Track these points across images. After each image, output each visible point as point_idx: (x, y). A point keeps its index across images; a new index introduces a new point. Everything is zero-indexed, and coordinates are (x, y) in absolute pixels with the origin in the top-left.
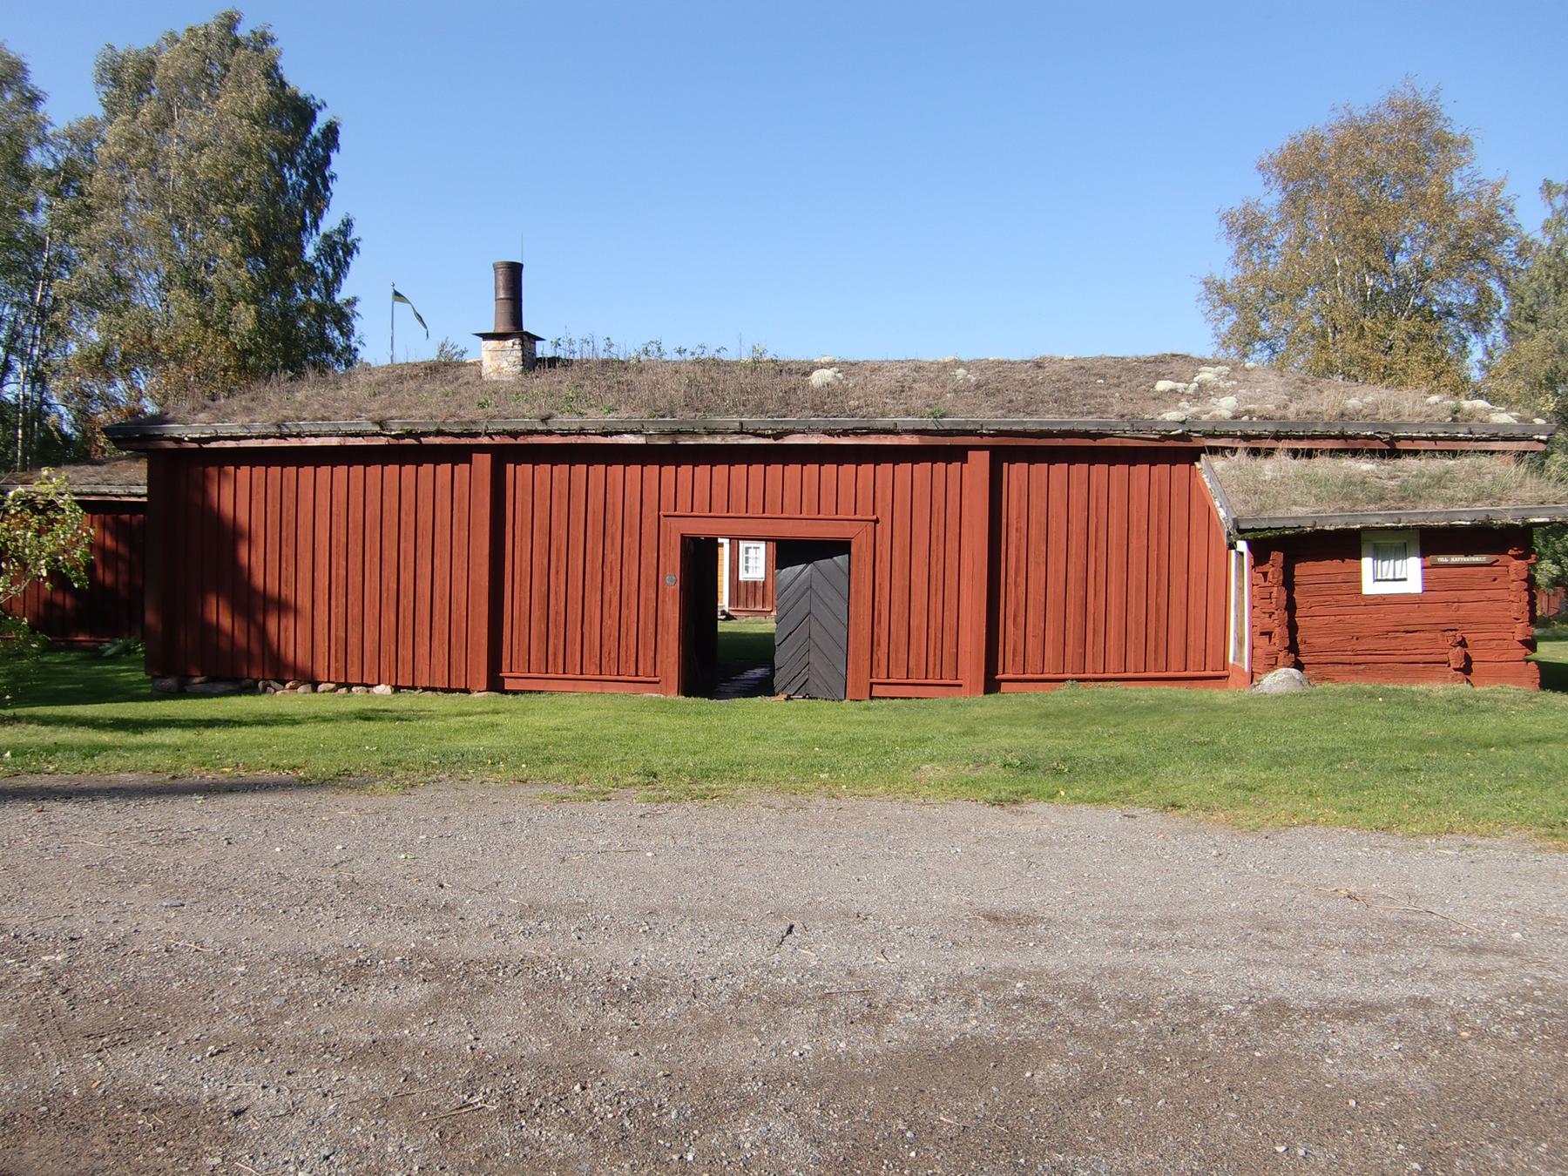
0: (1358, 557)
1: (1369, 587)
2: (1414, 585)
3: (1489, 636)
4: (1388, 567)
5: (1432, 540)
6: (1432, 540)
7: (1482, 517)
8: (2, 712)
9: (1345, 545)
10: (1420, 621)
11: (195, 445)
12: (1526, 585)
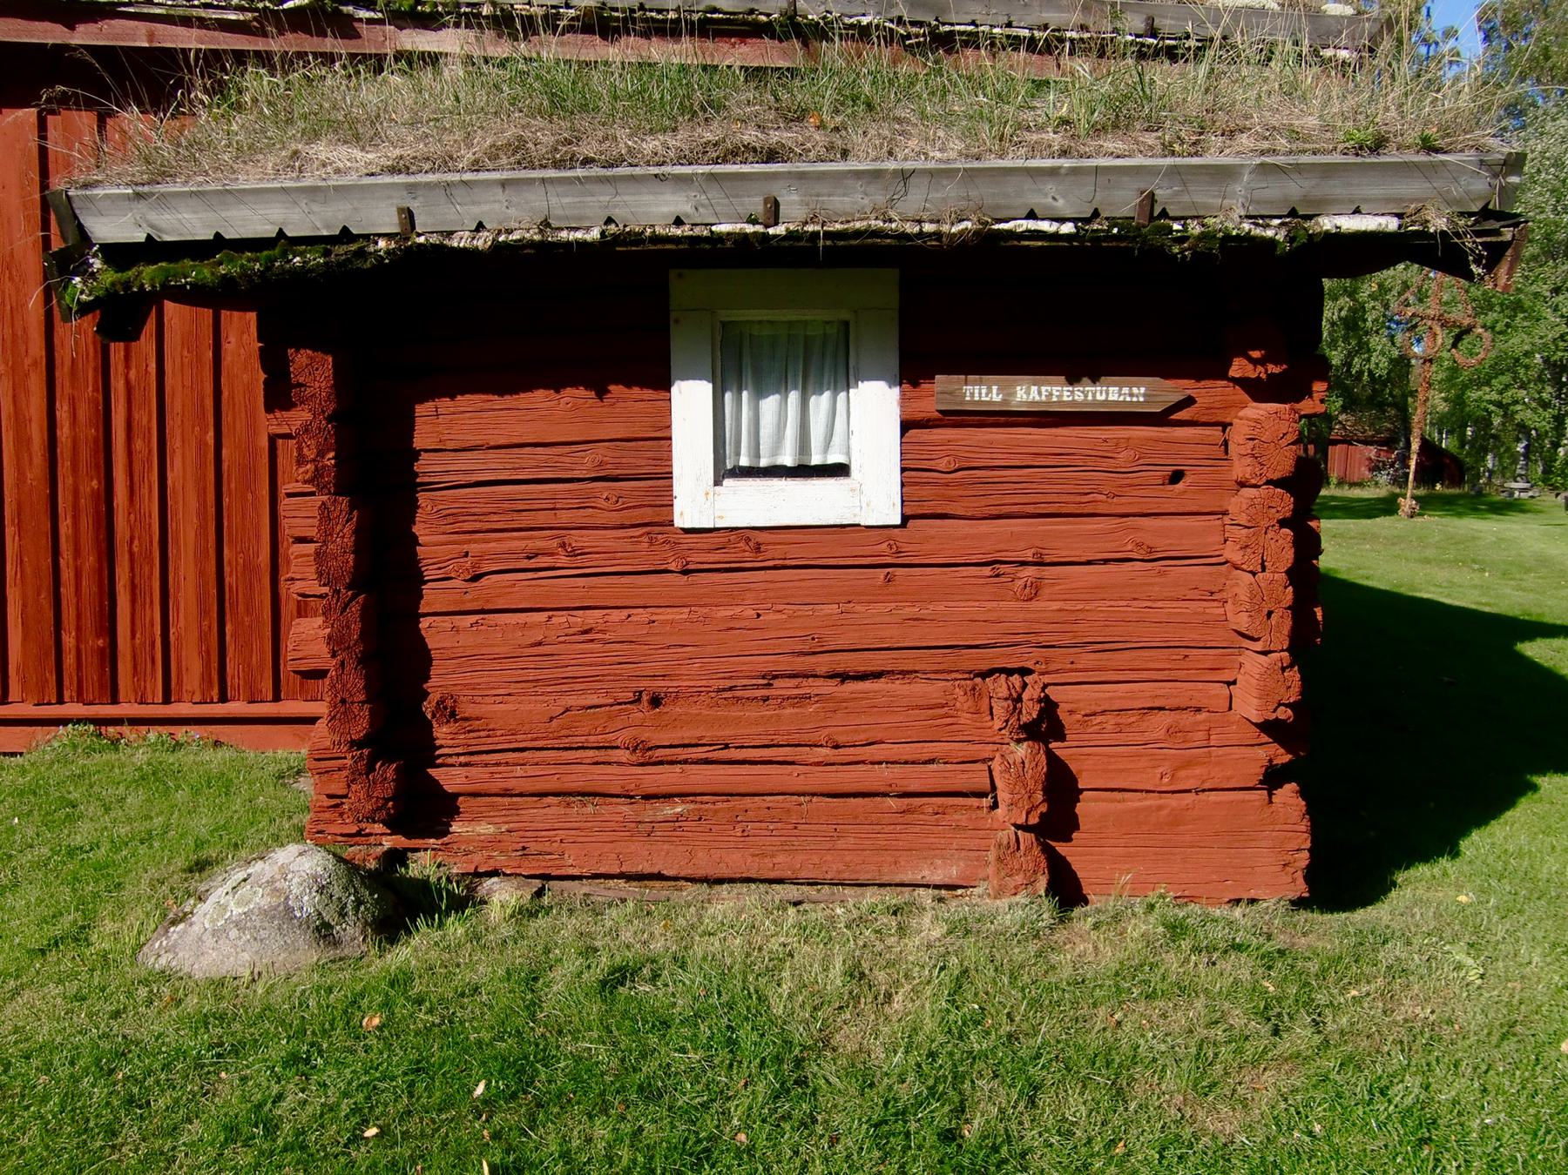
0: (658, 378)
1: (699, 500)
2: (872, 495)
3: (1145, 694)
4: (773, 420)
5: (952, 305)
6: (952, 305)
7: (1123, 203)
8: (1555, 550)
9: (603, 316)
10: (893, 635)
11: (672, 247)
12: (1285, 504)
